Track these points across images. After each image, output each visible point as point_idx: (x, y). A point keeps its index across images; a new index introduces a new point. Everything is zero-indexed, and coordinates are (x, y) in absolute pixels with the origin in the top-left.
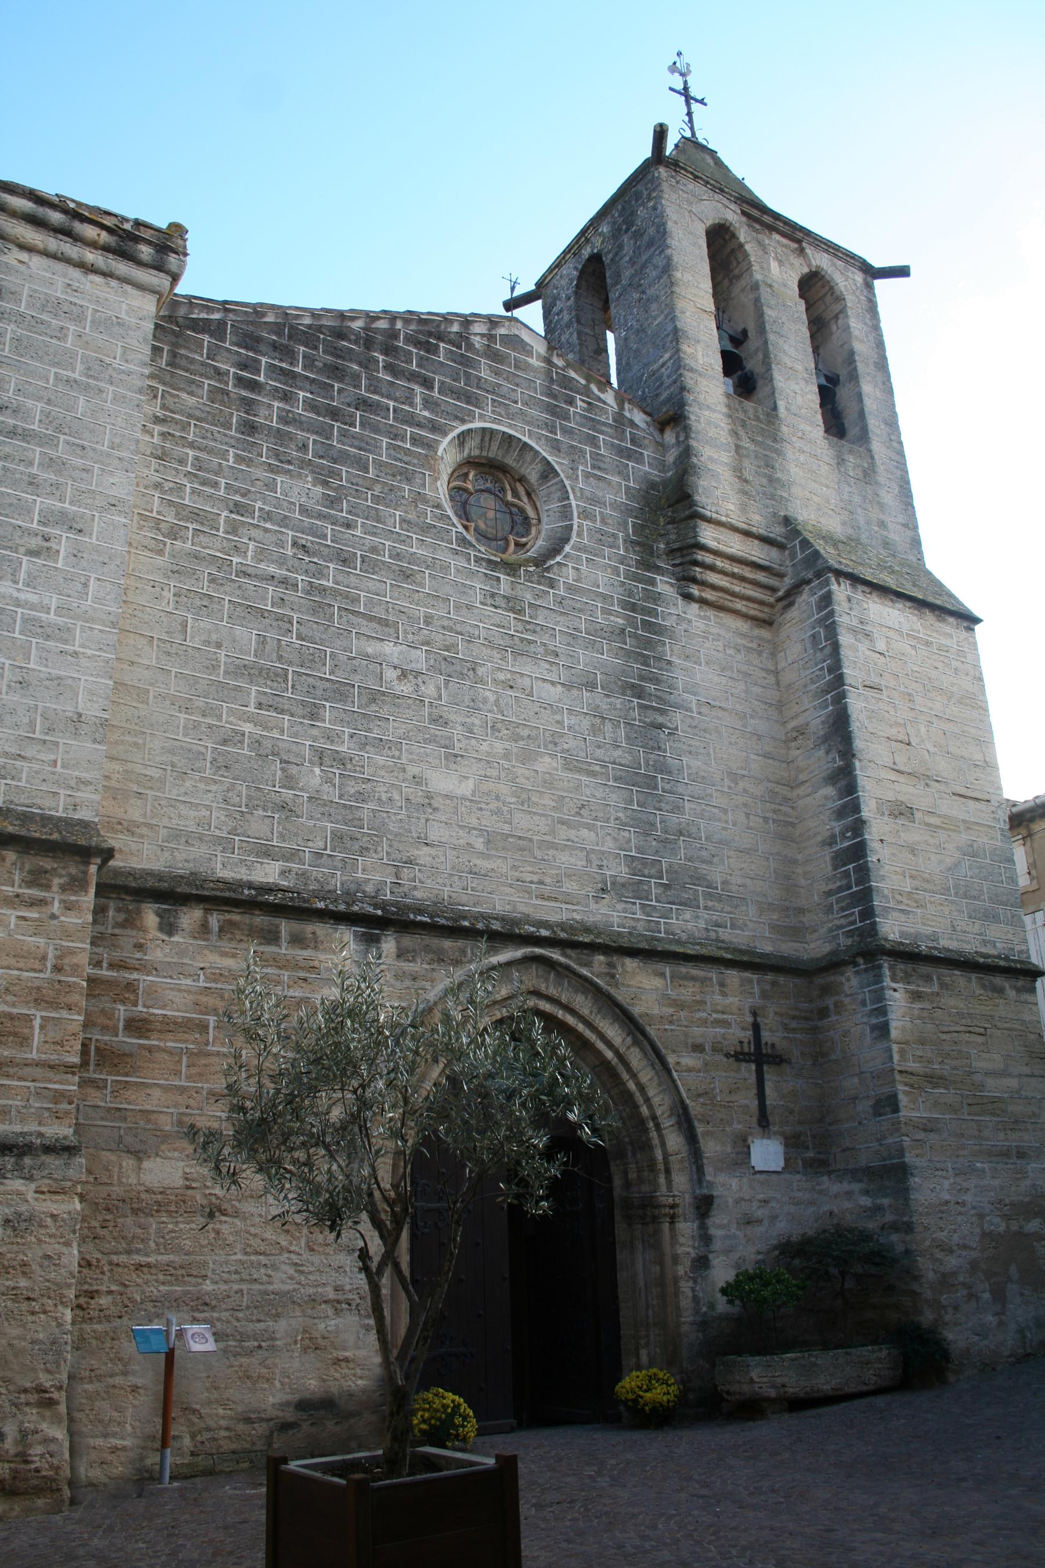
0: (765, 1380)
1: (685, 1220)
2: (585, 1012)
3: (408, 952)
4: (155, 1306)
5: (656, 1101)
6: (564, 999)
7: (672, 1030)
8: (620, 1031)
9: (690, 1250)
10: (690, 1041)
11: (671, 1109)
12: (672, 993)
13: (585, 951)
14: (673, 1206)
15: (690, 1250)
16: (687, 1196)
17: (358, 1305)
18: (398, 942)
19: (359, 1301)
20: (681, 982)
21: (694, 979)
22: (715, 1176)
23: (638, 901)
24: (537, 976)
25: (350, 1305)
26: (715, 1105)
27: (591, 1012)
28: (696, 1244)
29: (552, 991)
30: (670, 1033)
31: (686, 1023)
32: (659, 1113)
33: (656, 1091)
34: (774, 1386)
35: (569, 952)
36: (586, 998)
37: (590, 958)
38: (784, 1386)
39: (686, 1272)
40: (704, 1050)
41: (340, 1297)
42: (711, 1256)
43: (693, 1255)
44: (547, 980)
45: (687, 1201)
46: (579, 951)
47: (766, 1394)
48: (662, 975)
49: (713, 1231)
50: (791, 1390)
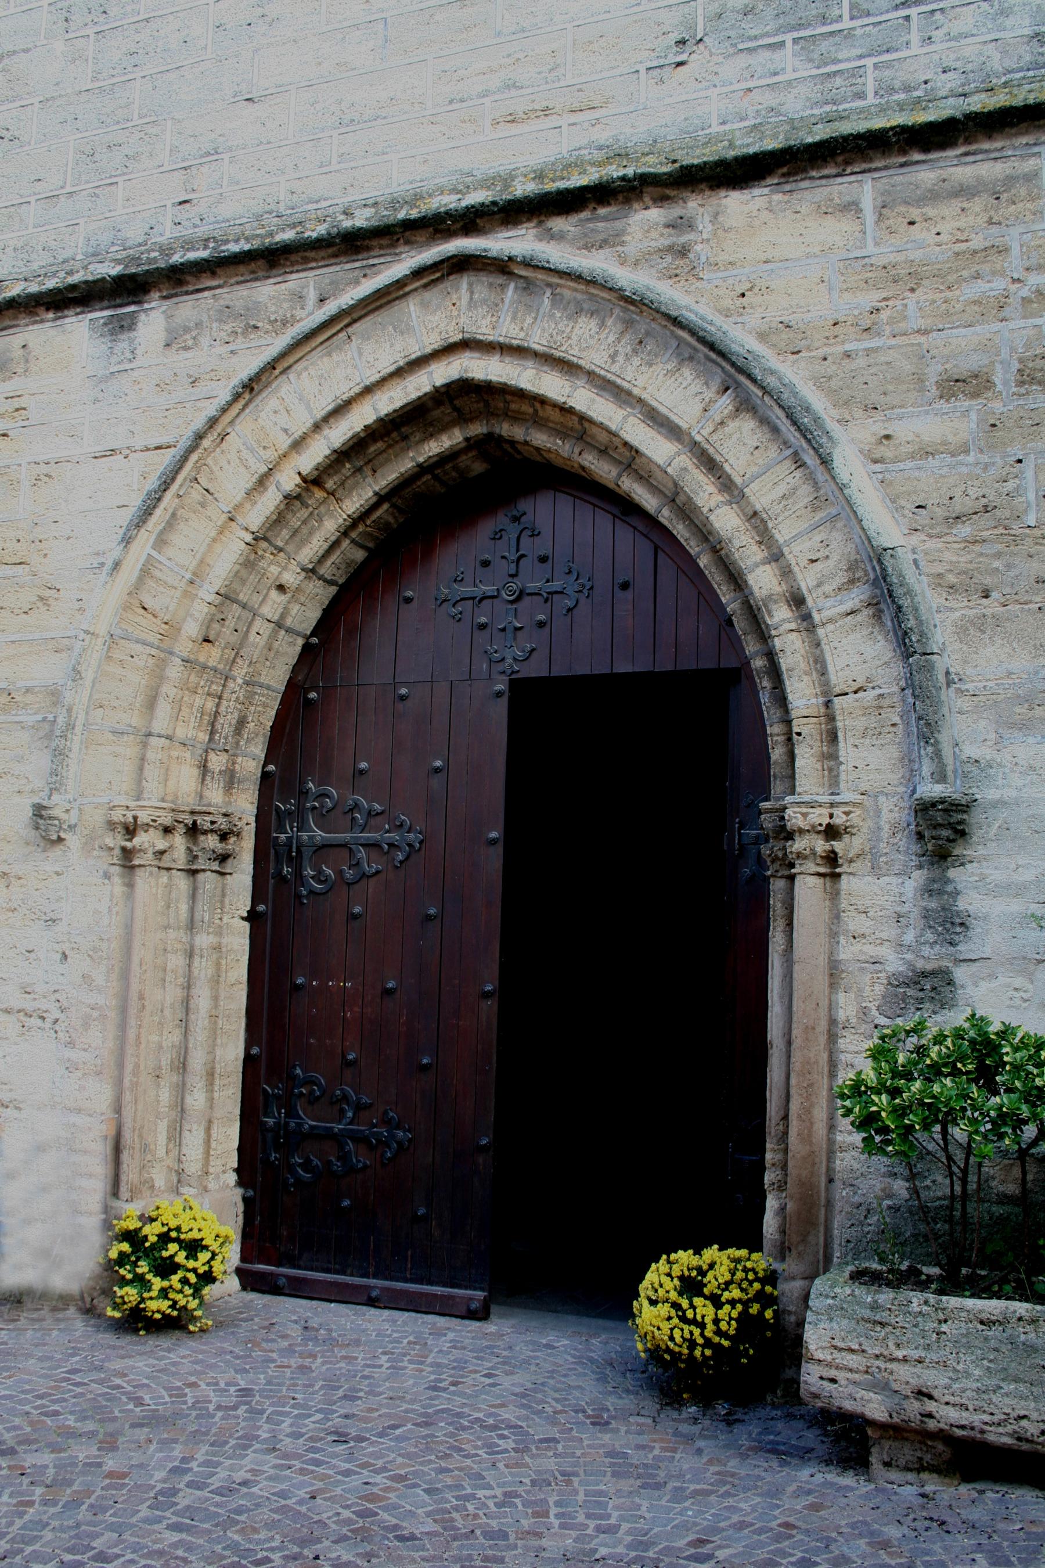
0: (852, 1360)
1: (876, 870)
2: (595, 359)
3: (187, 330)
4: (213, 823)
5: (797, 554)
6: (537, 341)
7: (868, 352)
8: (697, 386)
9: (886, 952)
10: (933, 372)
11: (852, 567)
12: (882, 252)
13: (602, 211)
14: (831, 832)
15: (886, 952)
16: (886, 804)
17: (56, 1021)
18: (169, 317)
19: (57, 1014)
20: (915, 213)
21: (964, 192)
22: (999, 743)
23: (788, 38)
24: (472, 304)
25: (43, 1018)
26: (1016, 540)
27: (613, 357)
28: (910, 937)
29: (508, 331)
30: (861, 362)
31: (922, 323)
32: (806, 580)
33: (803, 525)
34: (883, 1387)
35: (558, 224)
36: (602, 325)
37: (618, 225)
38: (922, 1394)
39: (865, 1011)
40: (989, 384)
41: (29, 1006)
42: (960, 974)
43: (895, 964)
44: (495, 307)
45: (885, 816)
46: (585, 214)
47: (848, 1405)
48: (852, 207)
49: (969, 902)
50: (953, 1415)
